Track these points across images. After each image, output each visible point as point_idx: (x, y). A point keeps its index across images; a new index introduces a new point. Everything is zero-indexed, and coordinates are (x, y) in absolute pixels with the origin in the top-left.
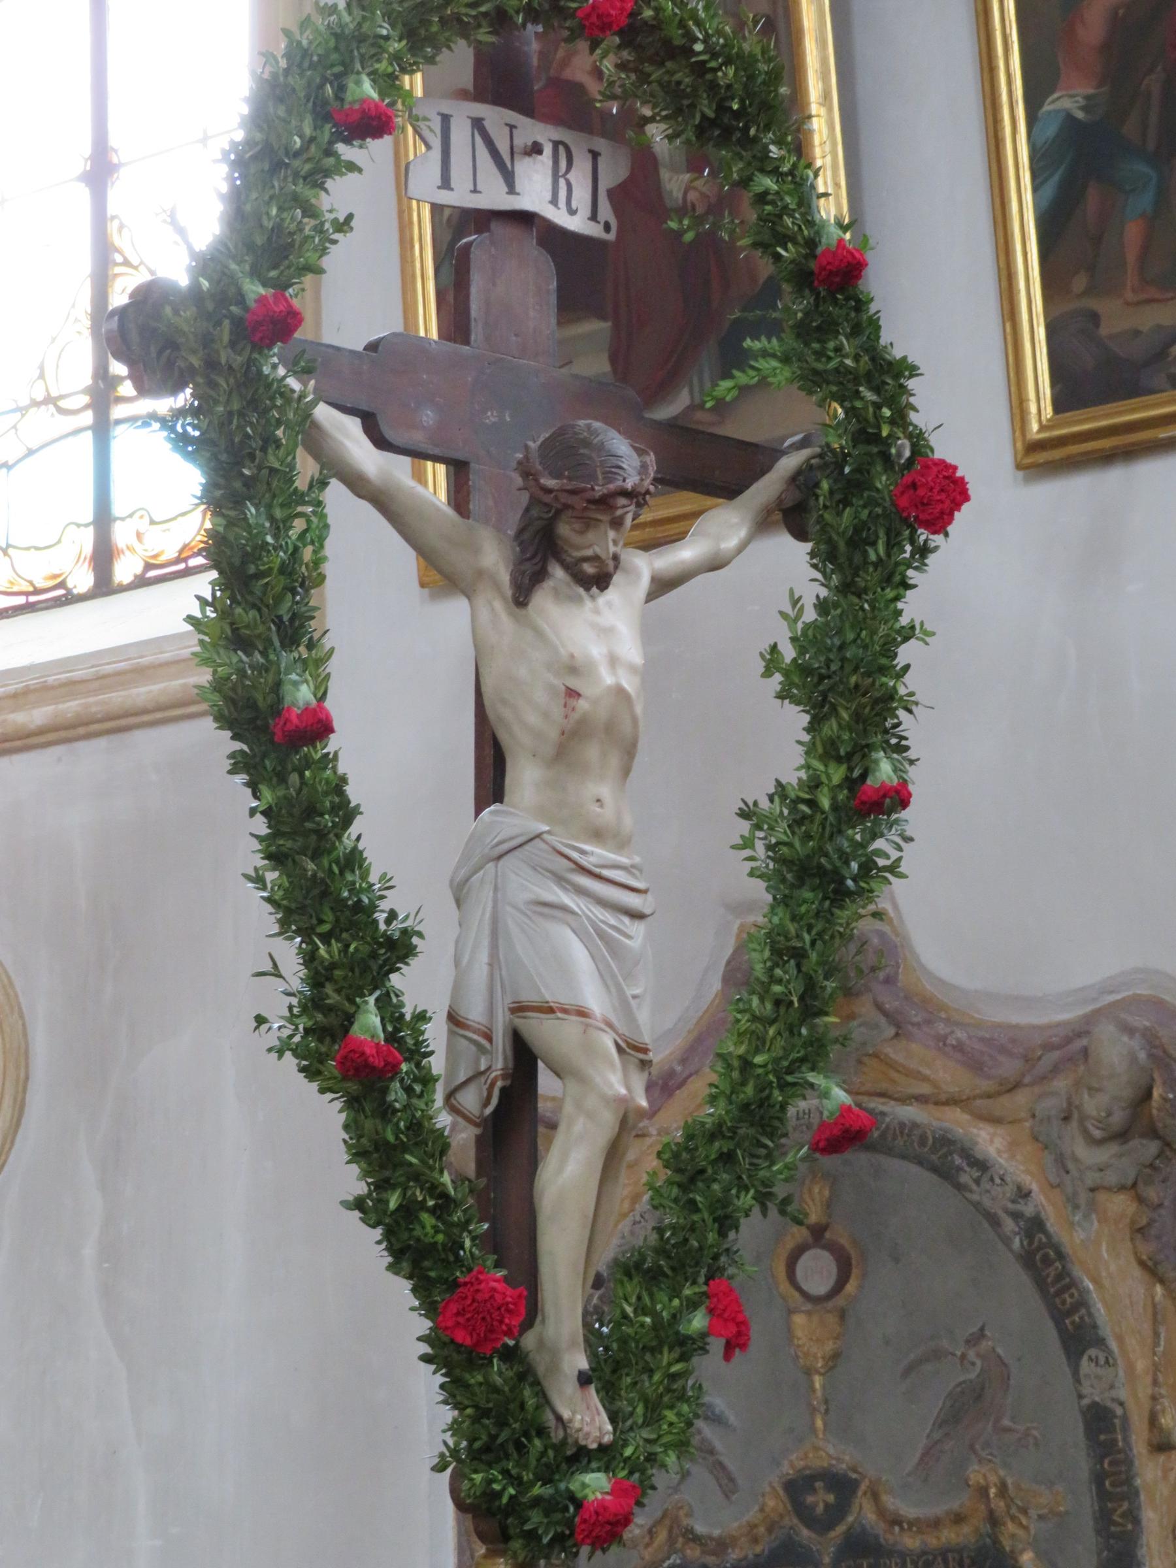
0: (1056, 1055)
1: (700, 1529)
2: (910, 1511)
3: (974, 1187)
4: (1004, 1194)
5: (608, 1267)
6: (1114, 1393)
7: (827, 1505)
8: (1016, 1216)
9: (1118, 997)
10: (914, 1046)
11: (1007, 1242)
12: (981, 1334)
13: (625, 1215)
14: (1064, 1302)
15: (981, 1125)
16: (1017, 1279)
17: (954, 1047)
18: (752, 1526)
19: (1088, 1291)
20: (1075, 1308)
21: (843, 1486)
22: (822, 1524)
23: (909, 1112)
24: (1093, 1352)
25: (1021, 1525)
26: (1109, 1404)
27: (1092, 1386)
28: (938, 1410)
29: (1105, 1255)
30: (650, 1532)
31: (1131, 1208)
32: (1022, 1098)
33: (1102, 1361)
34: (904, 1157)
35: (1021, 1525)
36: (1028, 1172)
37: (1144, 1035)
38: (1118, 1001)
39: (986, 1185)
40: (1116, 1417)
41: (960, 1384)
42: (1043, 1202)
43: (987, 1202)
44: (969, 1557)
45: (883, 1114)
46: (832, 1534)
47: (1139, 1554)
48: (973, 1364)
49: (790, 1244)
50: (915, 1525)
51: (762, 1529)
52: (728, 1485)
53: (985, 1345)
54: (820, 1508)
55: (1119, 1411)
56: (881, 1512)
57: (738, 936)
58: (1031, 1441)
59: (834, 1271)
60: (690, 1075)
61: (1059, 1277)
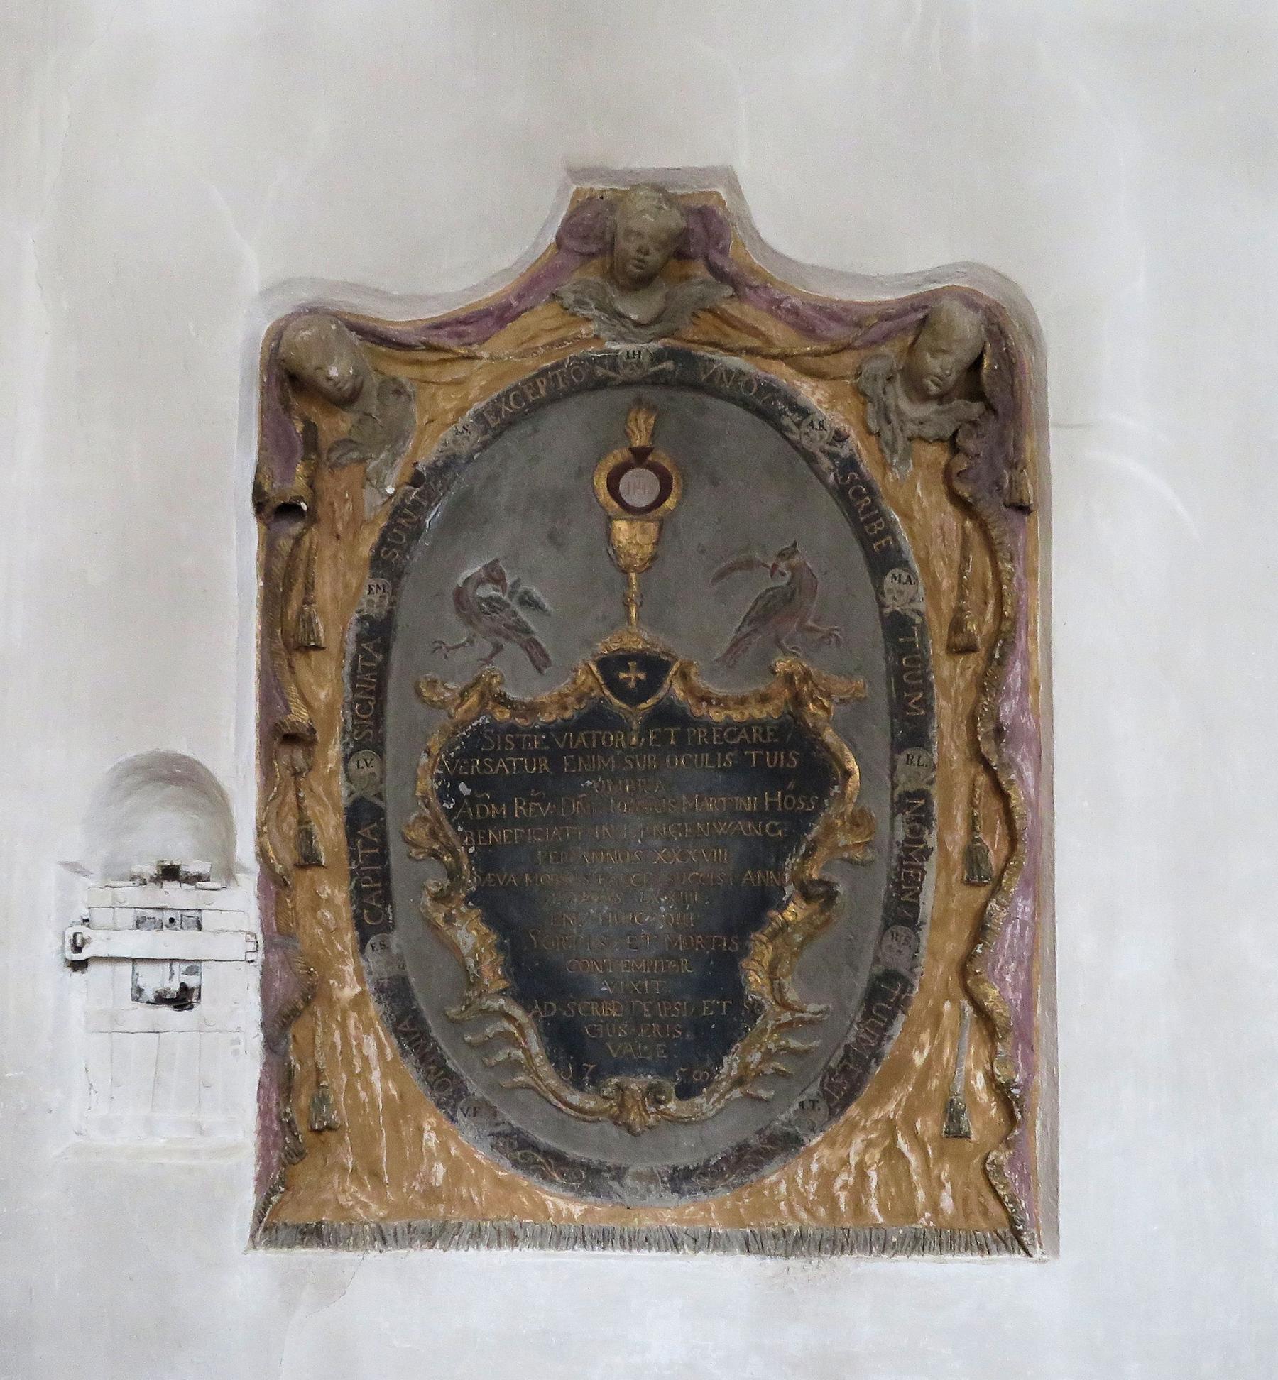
0: (887, 325)
1: (512, 695)
2: (717, 691)
3: (794, 428)
4: (822, 437)
5: (428, 468)
6: (914, 606)
7: (638, 680)
8: (832, 456)
9: (938, 286)
10: (746, 307)
11: (822, 478)
12: (793, 551)
13: (448, 425)
14: (872, 530)
15: (804, 379)
16: (828, 511)
17: (788, 310)
18: (562, 696)
19: (895, 522)
20: (881, 535)
21: (655, 667)
22: (633, 698)
23: (736, 362)
24: (897, 571)
25: (823, 707)
26: (908, 613)
27: (894, 599)
28: (748, 609)
29: (919, 491)
30: (462, 695)
31: (944, 458)
32: (849, 359)
33: (904, 579)
34: (730, 398)
35: (823, 707)
36: (847, 420)
37: (985, 313)
38: (937, 290)
39: (805, 429)
40: (914, 624)
41: (772, 589)
42: (856, 442)
43: (805, 442)
44: (772, 730)
45: (712, 361)
46: (643, 705)
47: (930, 734)
48: (783, 574)
49: (611, 462)
50: (721, 702)
51: (571, 699)
52: (539, 659)
53: (796, 560)
54: (632, 684)
55: (918, 620)
56: (690, 690)
57: (573, 199)
58: (833, 639)
59: (658, 488)
60: (526, 310)
61: (868, 509)
